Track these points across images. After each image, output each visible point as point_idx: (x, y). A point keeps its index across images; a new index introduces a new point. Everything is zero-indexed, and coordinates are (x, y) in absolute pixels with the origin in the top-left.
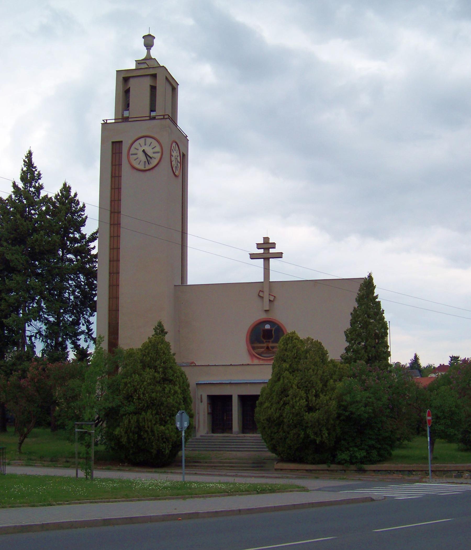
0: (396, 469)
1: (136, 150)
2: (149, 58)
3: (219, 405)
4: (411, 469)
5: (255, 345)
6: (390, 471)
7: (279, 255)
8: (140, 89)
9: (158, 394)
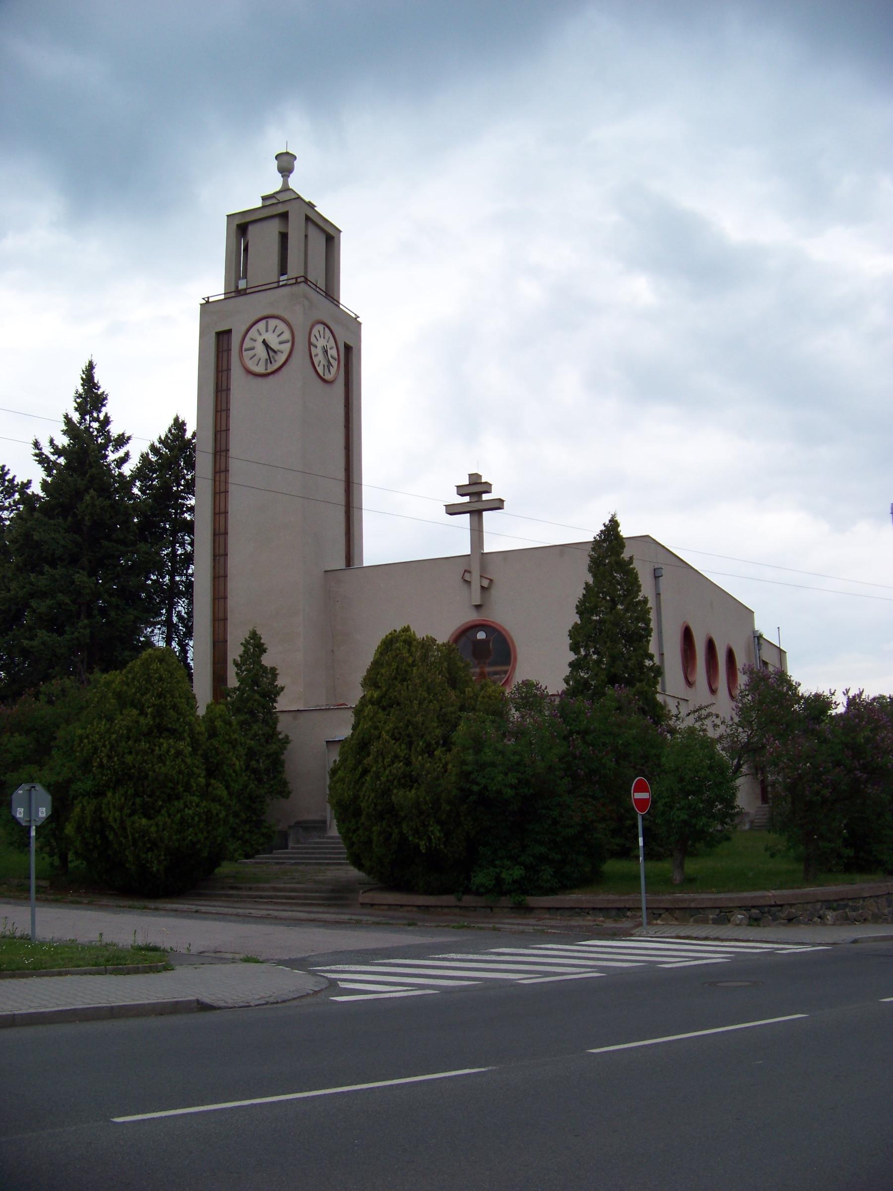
0: (591, 905)
1: (253, 342)
2: (286, 189)
4: (622, 906)
6: (581, 908)
7: (498, 505)
8: (264, 239)
9: (139, 757)
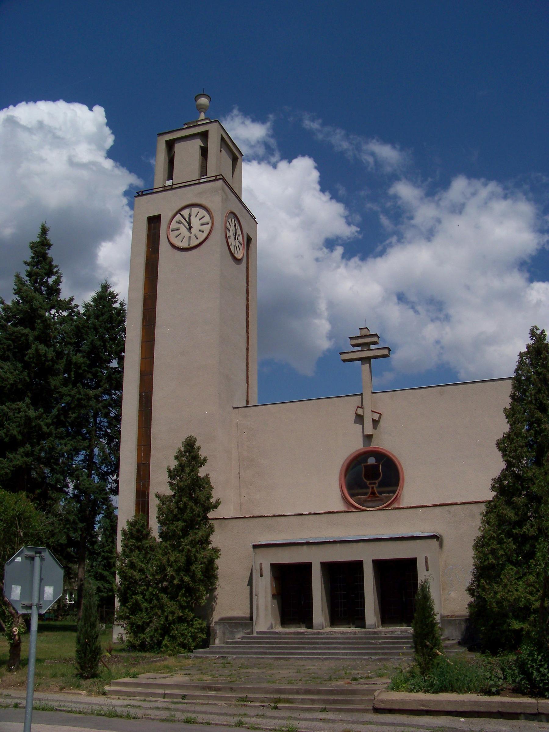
3: (291, 584)
5: (356, 491)
